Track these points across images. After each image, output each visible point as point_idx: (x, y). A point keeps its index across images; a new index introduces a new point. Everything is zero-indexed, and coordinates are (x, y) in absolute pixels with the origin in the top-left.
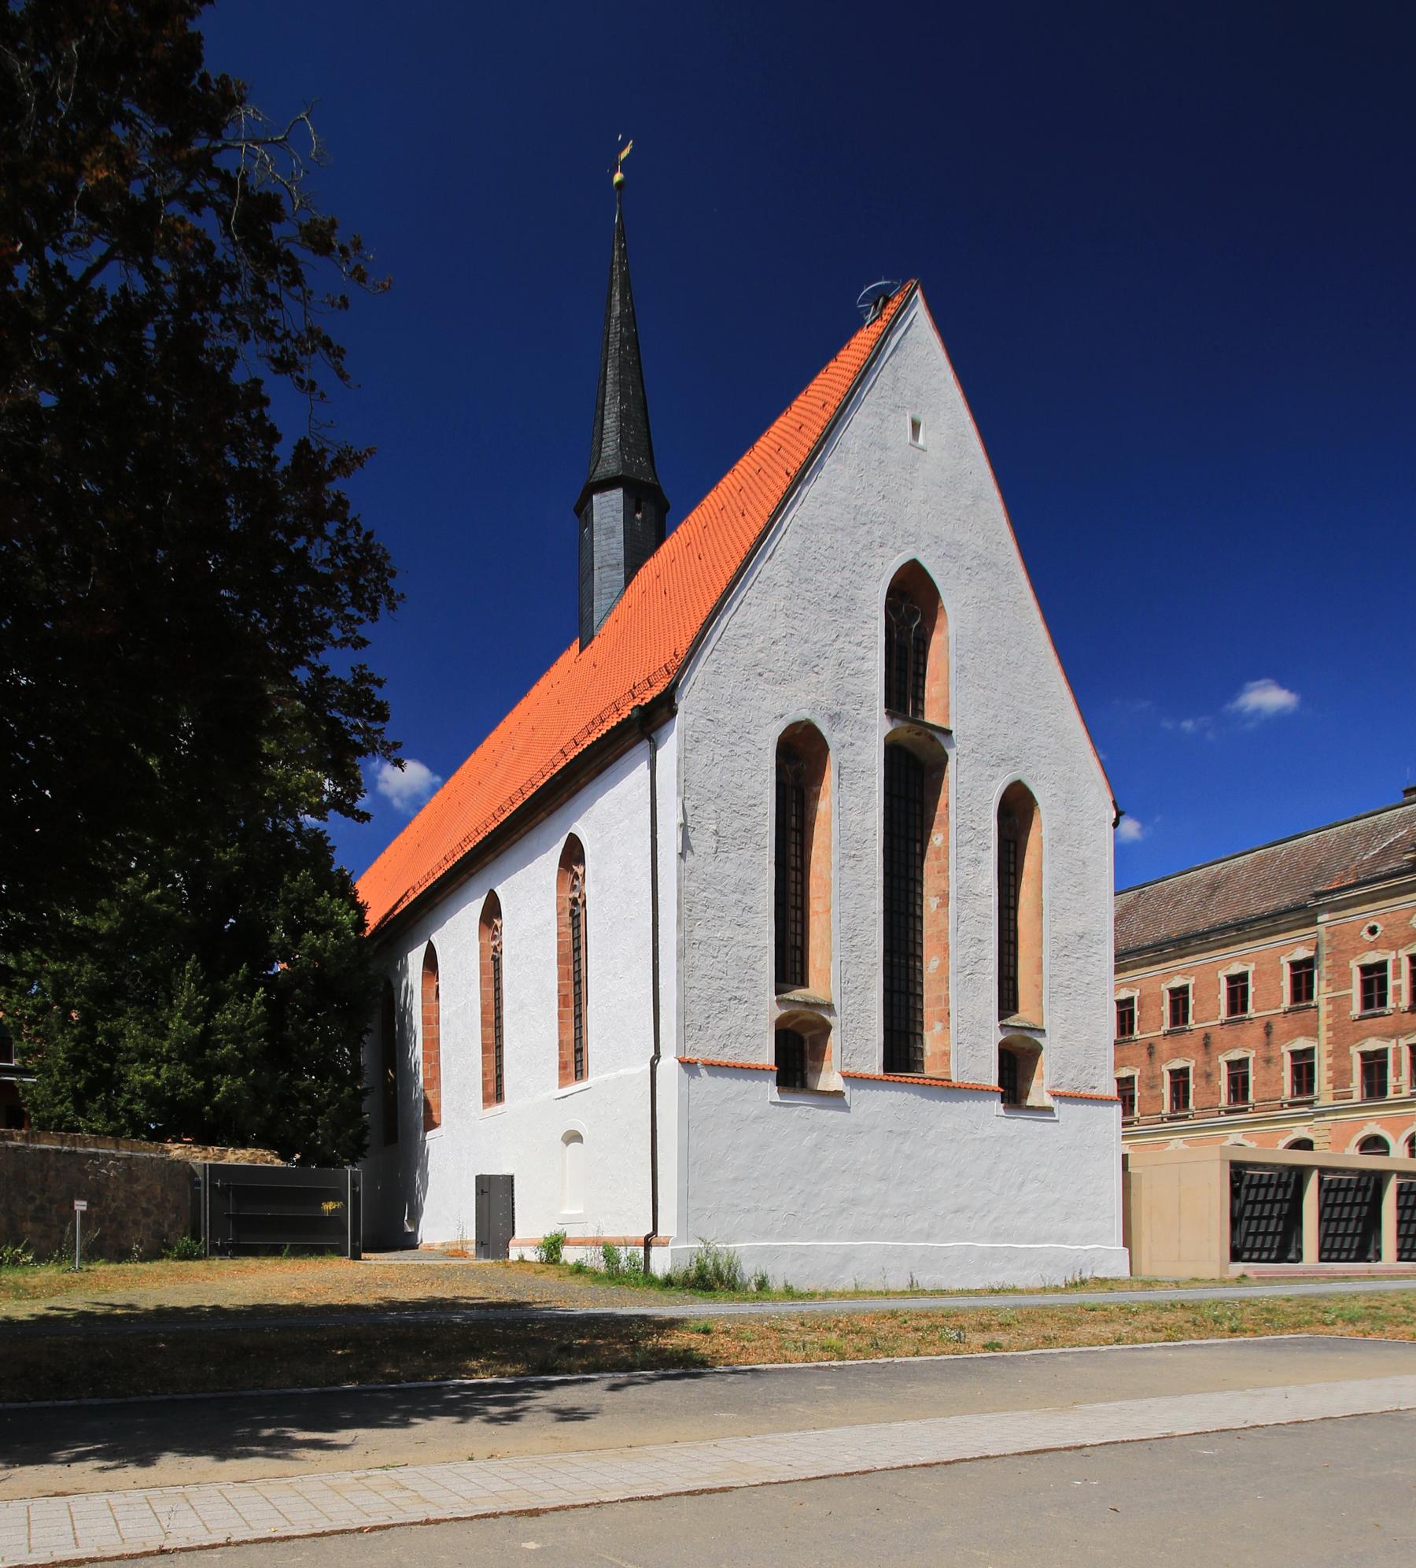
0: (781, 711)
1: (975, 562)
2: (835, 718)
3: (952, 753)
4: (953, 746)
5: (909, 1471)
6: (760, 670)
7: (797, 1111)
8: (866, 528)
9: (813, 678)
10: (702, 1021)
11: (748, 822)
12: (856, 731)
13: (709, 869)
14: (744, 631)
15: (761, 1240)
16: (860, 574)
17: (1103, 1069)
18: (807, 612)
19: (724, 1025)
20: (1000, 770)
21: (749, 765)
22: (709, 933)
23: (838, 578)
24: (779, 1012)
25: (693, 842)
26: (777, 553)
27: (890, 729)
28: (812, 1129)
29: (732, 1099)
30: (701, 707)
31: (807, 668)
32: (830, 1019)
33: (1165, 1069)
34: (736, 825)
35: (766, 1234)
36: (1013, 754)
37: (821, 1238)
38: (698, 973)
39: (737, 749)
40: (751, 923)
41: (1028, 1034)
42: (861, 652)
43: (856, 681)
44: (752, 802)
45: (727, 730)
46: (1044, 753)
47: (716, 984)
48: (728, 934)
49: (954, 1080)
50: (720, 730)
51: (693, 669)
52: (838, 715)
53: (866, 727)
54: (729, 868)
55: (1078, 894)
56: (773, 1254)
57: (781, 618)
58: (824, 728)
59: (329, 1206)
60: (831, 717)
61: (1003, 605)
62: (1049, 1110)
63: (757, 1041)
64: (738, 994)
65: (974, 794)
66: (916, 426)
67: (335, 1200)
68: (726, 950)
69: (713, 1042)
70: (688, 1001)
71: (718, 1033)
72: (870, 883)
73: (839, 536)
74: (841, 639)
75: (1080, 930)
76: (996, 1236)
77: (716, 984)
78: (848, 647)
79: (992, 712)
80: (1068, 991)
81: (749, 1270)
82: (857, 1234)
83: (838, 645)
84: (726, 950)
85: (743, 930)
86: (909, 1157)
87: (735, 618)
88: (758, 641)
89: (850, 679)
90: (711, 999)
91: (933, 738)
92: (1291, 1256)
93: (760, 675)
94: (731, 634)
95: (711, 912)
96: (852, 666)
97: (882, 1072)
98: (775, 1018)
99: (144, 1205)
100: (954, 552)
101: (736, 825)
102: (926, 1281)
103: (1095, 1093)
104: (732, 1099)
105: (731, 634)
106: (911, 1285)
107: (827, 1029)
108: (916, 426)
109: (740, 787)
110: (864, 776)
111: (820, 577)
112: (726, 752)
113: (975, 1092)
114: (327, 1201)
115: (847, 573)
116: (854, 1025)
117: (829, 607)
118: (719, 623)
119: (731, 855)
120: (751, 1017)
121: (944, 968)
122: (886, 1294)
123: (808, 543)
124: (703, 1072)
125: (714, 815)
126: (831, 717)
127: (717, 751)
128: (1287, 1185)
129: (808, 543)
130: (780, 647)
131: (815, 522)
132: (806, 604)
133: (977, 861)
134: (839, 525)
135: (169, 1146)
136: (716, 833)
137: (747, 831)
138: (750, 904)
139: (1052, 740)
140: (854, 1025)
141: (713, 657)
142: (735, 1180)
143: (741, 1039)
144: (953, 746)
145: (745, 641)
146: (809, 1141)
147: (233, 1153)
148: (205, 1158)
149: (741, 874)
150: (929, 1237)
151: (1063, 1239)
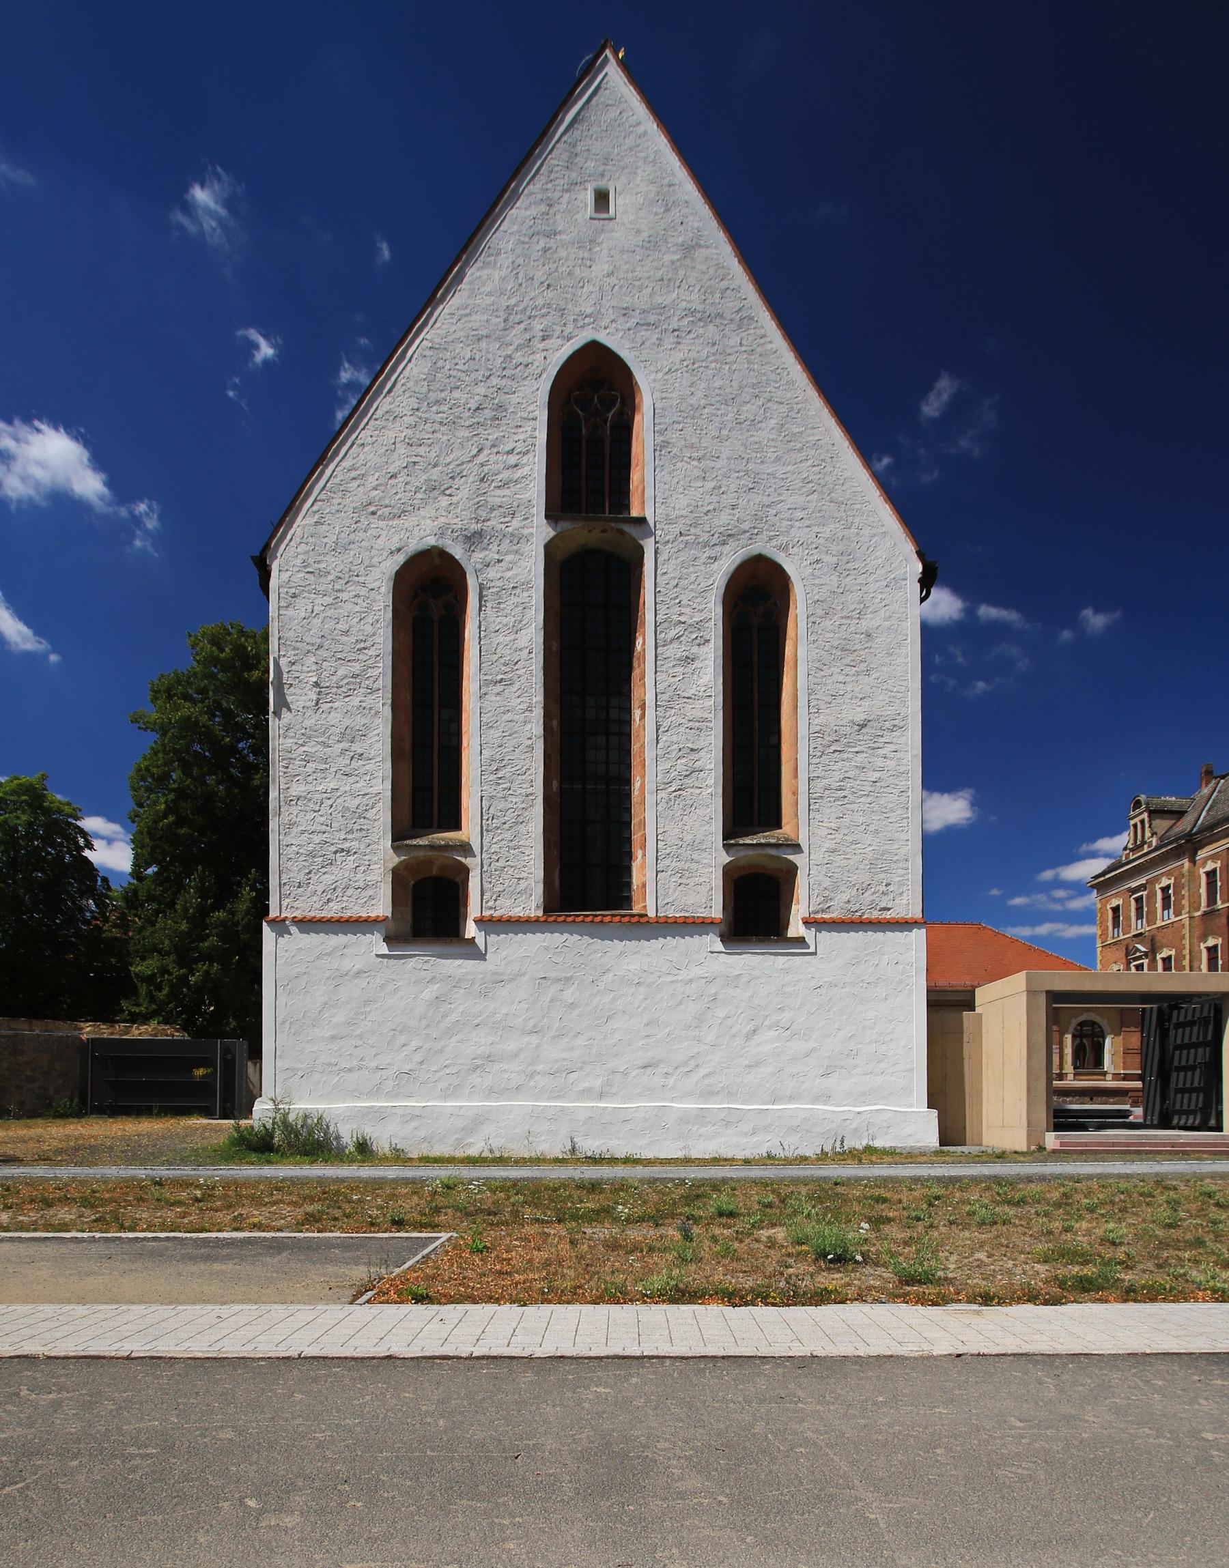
0: (398, 546)
1: (686, 321)
2: (474, 539)
3: (649, 546)
4: (651, 534)
5: (132, 1365)
6: (372, 509)
7: (412, 963)
8: (522, 326)
9: (444, 501)
10: (301, 877)
11: (356, 668)
12: (506, 545)
13: (308, 723)
14: (353, 474)
15: (497, 1100)
16: (513, 378)
17: (901, 884)
18: (439, 435)
19: (328, 879)
20: (727, 548)
21: (357, 608)
22: (310, 788)
23: (481, 390)
24: (396, 860)
25: (289, 699)
26: (399, 385)
27: (552, 533)
28: (432, 980)
29: (328, 954)
30: (298, 561)
31: (436, 493)
32: (467, 861)
33: (1202, 871)
34: (341, 673)
35: (376, 1092)
36: (746, 526)
37: (446, 1094)
38: (295, 830)
39: (344, 596)
40: (362, 770)
41: (773, 852)
42: (512, 459)
43: (506, 492)
44: (362, 645)
45: (330, 577)
46: (799, 514)
47: (317, 839)
48: (332, 786)
49: (651, 914)
50: (322, 580)
51: (290, 526)
52: (479, 534)
53: (518, 539)
54: (334, 718)
55: (858, 674)
56: (380, 1116)
57: (402, 449)
58: (457, 552)
59: (200, 1072)
60: (468, 539)
61: (732, 358)
62: (801, 941)
63: (370, 892)
64: (346, 845)
65: (683, 583)
66: (602, 199)
67: (205, 1067)
68: (330, 802)
69: (315, 898)
70: (284, 858)
71: (320, 888)
72: (524, 706)
73: (483, 345)
74: (486, 452)
75: (859, 718)
76: (709, 1094)
77: (317, 839)
78: (493, 458)
79: (712, 484)
80: (843, 793)
81: (347, 1135)
82: (491, 1092)
83: (481, 458)
84: (330, 802)
85: (353, 779)
86: (573, 1005)
87: (344, 464)
88: (371, 481)
89: (498, 492)
90: (311, 854)
91: (621, 532)
92: (1212, 1122)
93: (373, 513)
94: (336, 481)
95: (311, 767)
96: (500, 477)
97: (540, 913)
98: (391, 866)
99: (29, 1073)
100: (652, 318)
101: (341, 673)
102: (590, 1145)
103: (887, 915)
104: (328, 954)
105: (336, 481)
106: (573, 1150)
107: (792, 870)
108: (602, 199)
109: (346, 633)
110: (517, 591)
111: (456, 394)
112: (328, 600)
113: (904, 925)
114: (198, 1067)
115: (494, 381)
116: (502, 863)
117: (467, 424)
118: (322, 473)
119: (336, 705)
120: (362, 868)
121: (643, 786)
122: (538, 1161)
123: (440, 363)
124: (294, 929)
125: (314, 667)
126: (468, 539)
127: (317, 602)
128: (1206, 1021)
129: (440, 363)
130: (401, 478)
131: (450, 338)
132: (437, 426)
133: (689, 660)
134: (484, 333)
135: (82, 1024)
136: (316, 684)
137: (355, 676)
138: (359, 751)
139: (814, 497)
140: (502, 863)
141: (315, 508)
142: (333, 1038)
143: (350, 892)
144: (651, 534)
145: (355, 484)
146: (429, 993)
147: (138, 1028)
148: (112, 1034)
149: (347, 722)
150: (601, 1096)
151: (825, 1097)
